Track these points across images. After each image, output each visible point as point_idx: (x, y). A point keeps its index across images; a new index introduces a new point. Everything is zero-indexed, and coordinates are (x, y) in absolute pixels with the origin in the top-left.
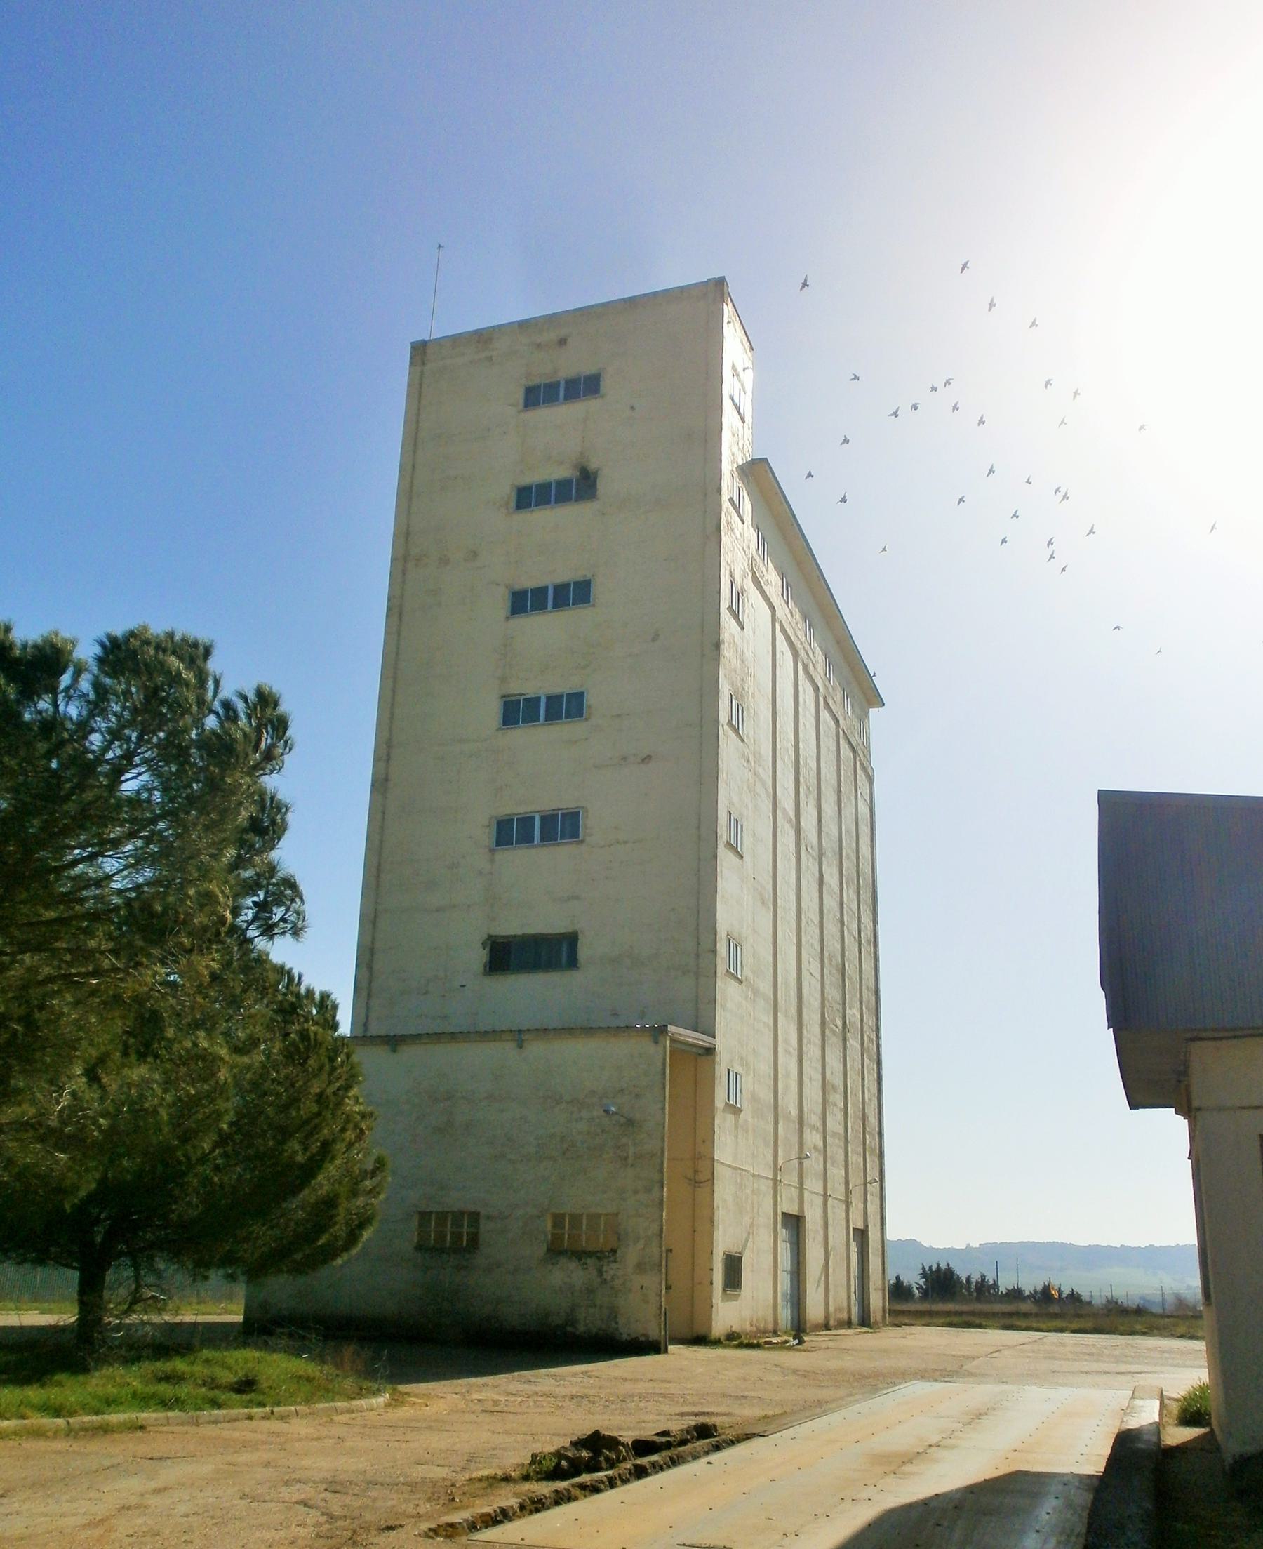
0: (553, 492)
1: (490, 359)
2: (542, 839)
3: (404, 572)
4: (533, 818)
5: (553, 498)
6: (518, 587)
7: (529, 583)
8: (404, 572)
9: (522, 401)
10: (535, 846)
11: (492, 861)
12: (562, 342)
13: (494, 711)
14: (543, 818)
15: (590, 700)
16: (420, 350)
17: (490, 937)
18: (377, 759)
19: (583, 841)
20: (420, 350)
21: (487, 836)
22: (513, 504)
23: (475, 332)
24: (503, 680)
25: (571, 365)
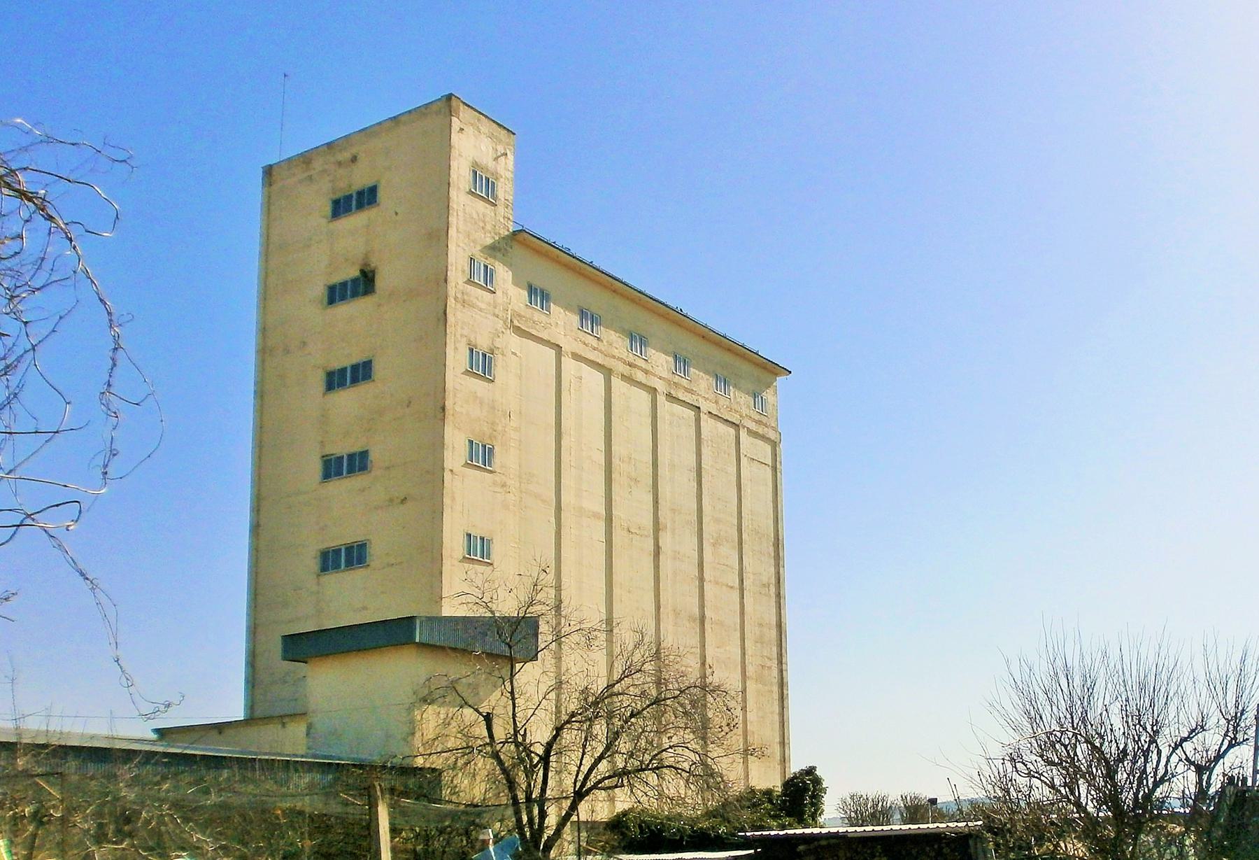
0: (345, 464)
1: (310, 178)
2: (349, 472)
3: (263, 361)
6: (329, 369)
7: (337, 365)
8: (263, 361)
9: (330, 214)
11: (318, 584)
12: (354, 159)
13: (317, 468)
14: (347, 549)
15: (373, 456)
16: (268, 171)
18: (252, 510)
20: (268, 171)
21: (314, 564)
22: (326, 300)
25: (360, 179)
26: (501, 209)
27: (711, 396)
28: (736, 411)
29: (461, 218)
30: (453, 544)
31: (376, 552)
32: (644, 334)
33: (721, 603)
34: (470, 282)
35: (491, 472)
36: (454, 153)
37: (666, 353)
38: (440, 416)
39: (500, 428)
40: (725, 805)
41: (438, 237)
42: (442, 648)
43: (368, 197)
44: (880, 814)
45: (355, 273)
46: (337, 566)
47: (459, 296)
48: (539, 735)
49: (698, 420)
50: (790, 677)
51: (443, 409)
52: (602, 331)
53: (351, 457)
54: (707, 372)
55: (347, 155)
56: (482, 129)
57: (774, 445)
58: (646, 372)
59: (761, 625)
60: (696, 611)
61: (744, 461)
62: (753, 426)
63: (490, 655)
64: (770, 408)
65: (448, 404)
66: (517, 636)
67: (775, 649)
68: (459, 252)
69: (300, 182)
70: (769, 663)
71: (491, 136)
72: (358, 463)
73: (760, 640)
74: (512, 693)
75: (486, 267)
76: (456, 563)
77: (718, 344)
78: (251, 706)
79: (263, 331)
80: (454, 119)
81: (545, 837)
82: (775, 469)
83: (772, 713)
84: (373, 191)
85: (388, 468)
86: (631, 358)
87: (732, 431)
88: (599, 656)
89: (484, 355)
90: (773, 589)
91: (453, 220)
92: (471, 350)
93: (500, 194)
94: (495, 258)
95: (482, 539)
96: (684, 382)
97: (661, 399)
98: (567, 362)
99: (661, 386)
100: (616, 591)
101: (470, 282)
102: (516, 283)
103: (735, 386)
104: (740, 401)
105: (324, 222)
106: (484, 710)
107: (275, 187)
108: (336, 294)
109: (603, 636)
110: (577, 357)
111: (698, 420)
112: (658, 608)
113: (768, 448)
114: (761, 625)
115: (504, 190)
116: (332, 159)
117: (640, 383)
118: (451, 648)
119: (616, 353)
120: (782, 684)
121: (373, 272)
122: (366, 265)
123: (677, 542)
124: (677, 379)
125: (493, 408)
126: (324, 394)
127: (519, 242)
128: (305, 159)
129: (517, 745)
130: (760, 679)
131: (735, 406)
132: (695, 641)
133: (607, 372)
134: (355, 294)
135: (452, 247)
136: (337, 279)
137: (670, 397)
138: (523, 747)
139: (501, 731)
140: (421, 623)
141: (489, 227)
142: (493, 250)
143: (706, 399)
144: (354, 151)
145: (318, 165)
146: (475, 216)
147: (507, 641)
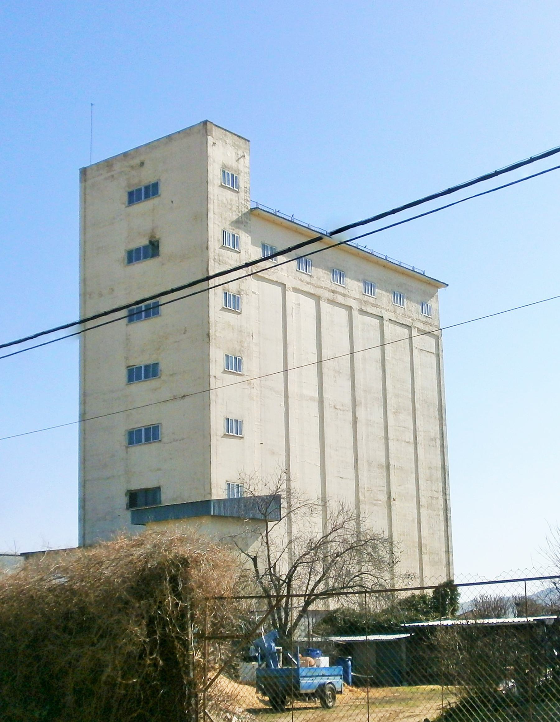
1: (113, 176)
4: (141, 430)
5: (143, 196)
8: (85, 302)
9: (127, 203)
10: (142, 381)
11: (127, 452)
12: (142, 164)
13: (123, 374)
15: (162, 367)
16: (84, 172)
17: (128, 491)
18: (80, 404)
19: (160, 441)
20: (84, 172)
21: (123, 439)
22: (126, 261)
23: (106, 161)
24: (127, 358)
25: (146, 177)
26: (242, 194)
27: (391, 308)
28: (409, 317)
29: (216, 204)
30: (217, 425)
31: (165, 432)
32: (340, 268)
33: (401, 454)
34: (223, 247)
35: (241, 375)
36: (210, 161)
37: (358, 280)
38: (207, 340)
39: (246, 345)
40: (393, 607)
41: (201, 217)
42: (226, 517)
43: (152, 190)
44: (497, 607)
45: (145, 242)
46: (139, 441)
47: (216, 257)
48: (283, 570)
49: (382, 326)
50: (452, 504)
51: (208, 335)
52: (313, 270)
53: (147, 367)
54: (387, 291)
55: (137, 161)
56: (228, 141)
57: (437, 339)
58: (344, 295)
59: (430, 468)
60: (383, 461)
61: (415, 352)
62: (421, 326)
63: (253, 519)
64: (433, 312)
65: (212, 332)
66: (269, 510)
67: (441, 485)
68: (216, 226)
69: (106, 179)
70: (436, 495)
71: (234, 145)
72: (151, 371)
73: (430, 479)
74: (267, 543)
75: (233, 236)
76: (219, 438)
77: (395, 271)
78: (83, 536)
79: (84, 281)
80: (209, 137)
81: (289, 626)
82: (438, 355)
83: (439, 530)
84: (155, 186)
85: (172, 375)
86: (334, 287)
87: (406, 331)
88: (318, 520)
89: (234, 296)
90: (438, 442)
91: (211, 206)
92: (226, 294)
93: (242, 184)
94: (239, 228)
95: (236, 421)
96: (371, 300)
97: (355, 313)
98: (290, 295)
99: (355, 305)
100: (327, 450)
101: (223, 247)
102: (254, 243)
103: (408, 298)
104: (411, 309)
105: (124, 206)
106: (253, 554)
107: (89, 183)
108: (133, 256)
109: (320, 508)
110: (296, 290)
111: (382, 326)
112: (357, 460)
113: (433, 341)
114: (430, 468)
115: (243, 182)
116: (126, 164)
117: (340, 304)
118: (230, 517)
119: (323, 284)
120: (446, 510)
121: (158, 242)
122: (152, 236)
123: (370, 414)
124: (366, 298)
125: (241, 331)
126: (127, 325)
127: (255, 215)
128: (109, 164)
129: (271, 574)
130: (430, 506)
131: (408, 313)
132: (384, 482)
133: (317, 299)
134: (146, 257)
135: (211, 225)
136: (134, 246)
137: (362, 312)
138: (275, 578)
139: (262, 567)
140: (214, 503)
141: (234, 208)
142: (238, 223)
143: (387, 310)
144: (142, 158)
145: (117, 167)
146: (225, 201)
147: (261, 510)
